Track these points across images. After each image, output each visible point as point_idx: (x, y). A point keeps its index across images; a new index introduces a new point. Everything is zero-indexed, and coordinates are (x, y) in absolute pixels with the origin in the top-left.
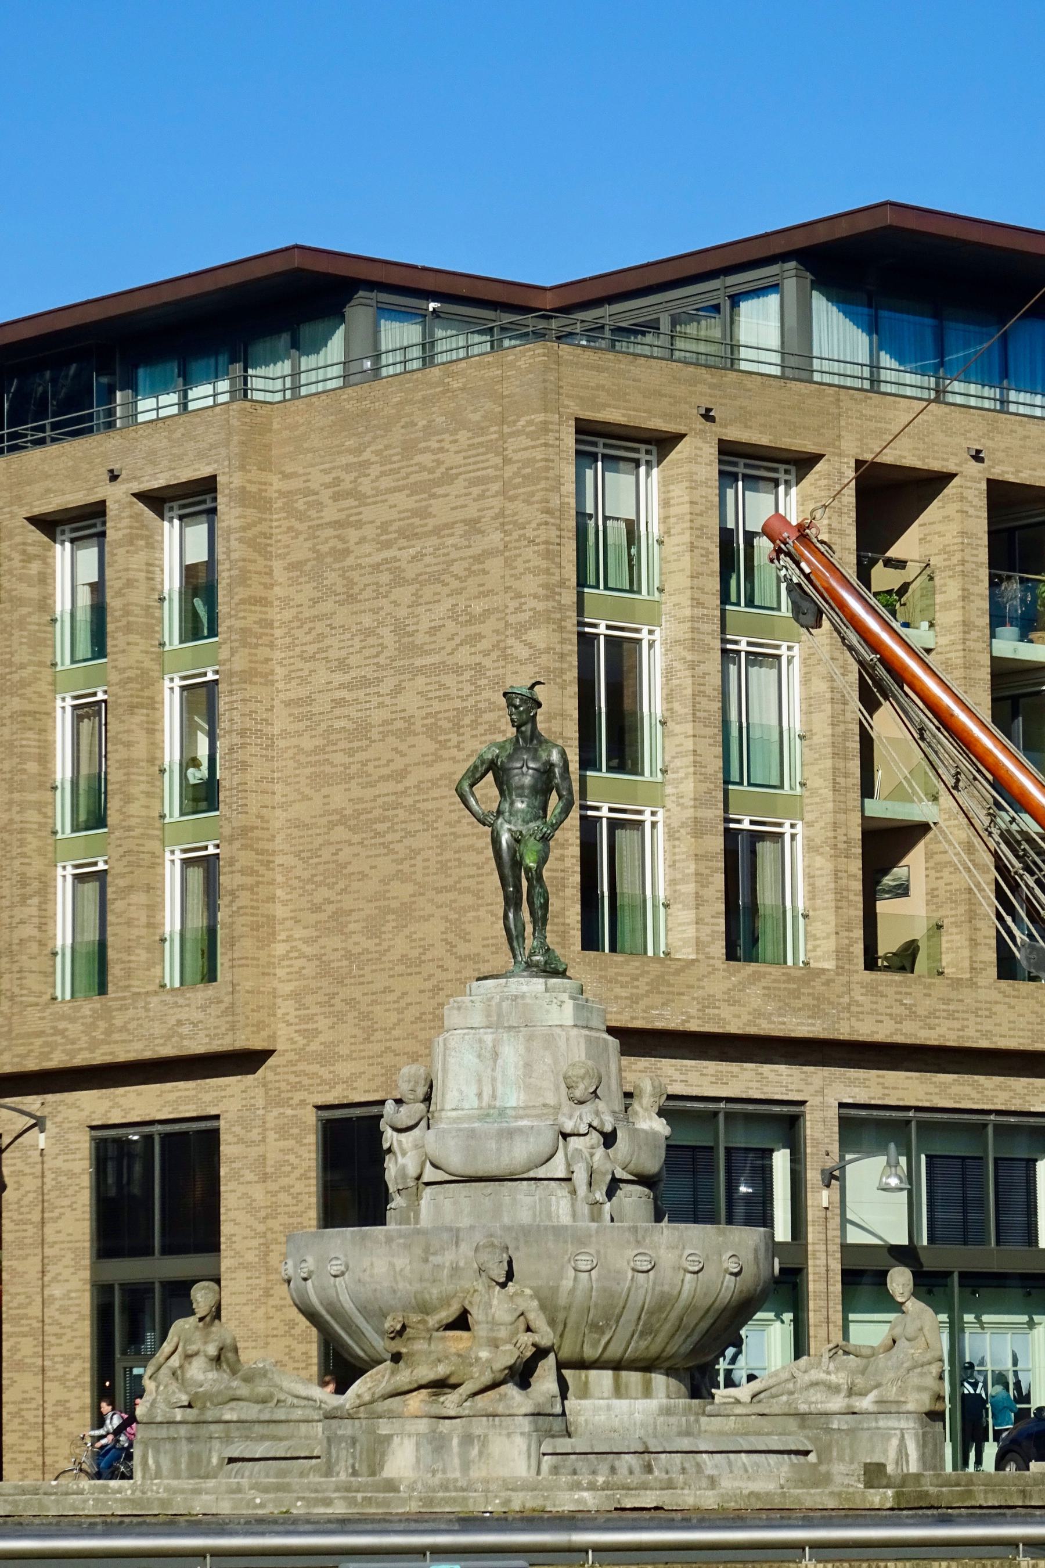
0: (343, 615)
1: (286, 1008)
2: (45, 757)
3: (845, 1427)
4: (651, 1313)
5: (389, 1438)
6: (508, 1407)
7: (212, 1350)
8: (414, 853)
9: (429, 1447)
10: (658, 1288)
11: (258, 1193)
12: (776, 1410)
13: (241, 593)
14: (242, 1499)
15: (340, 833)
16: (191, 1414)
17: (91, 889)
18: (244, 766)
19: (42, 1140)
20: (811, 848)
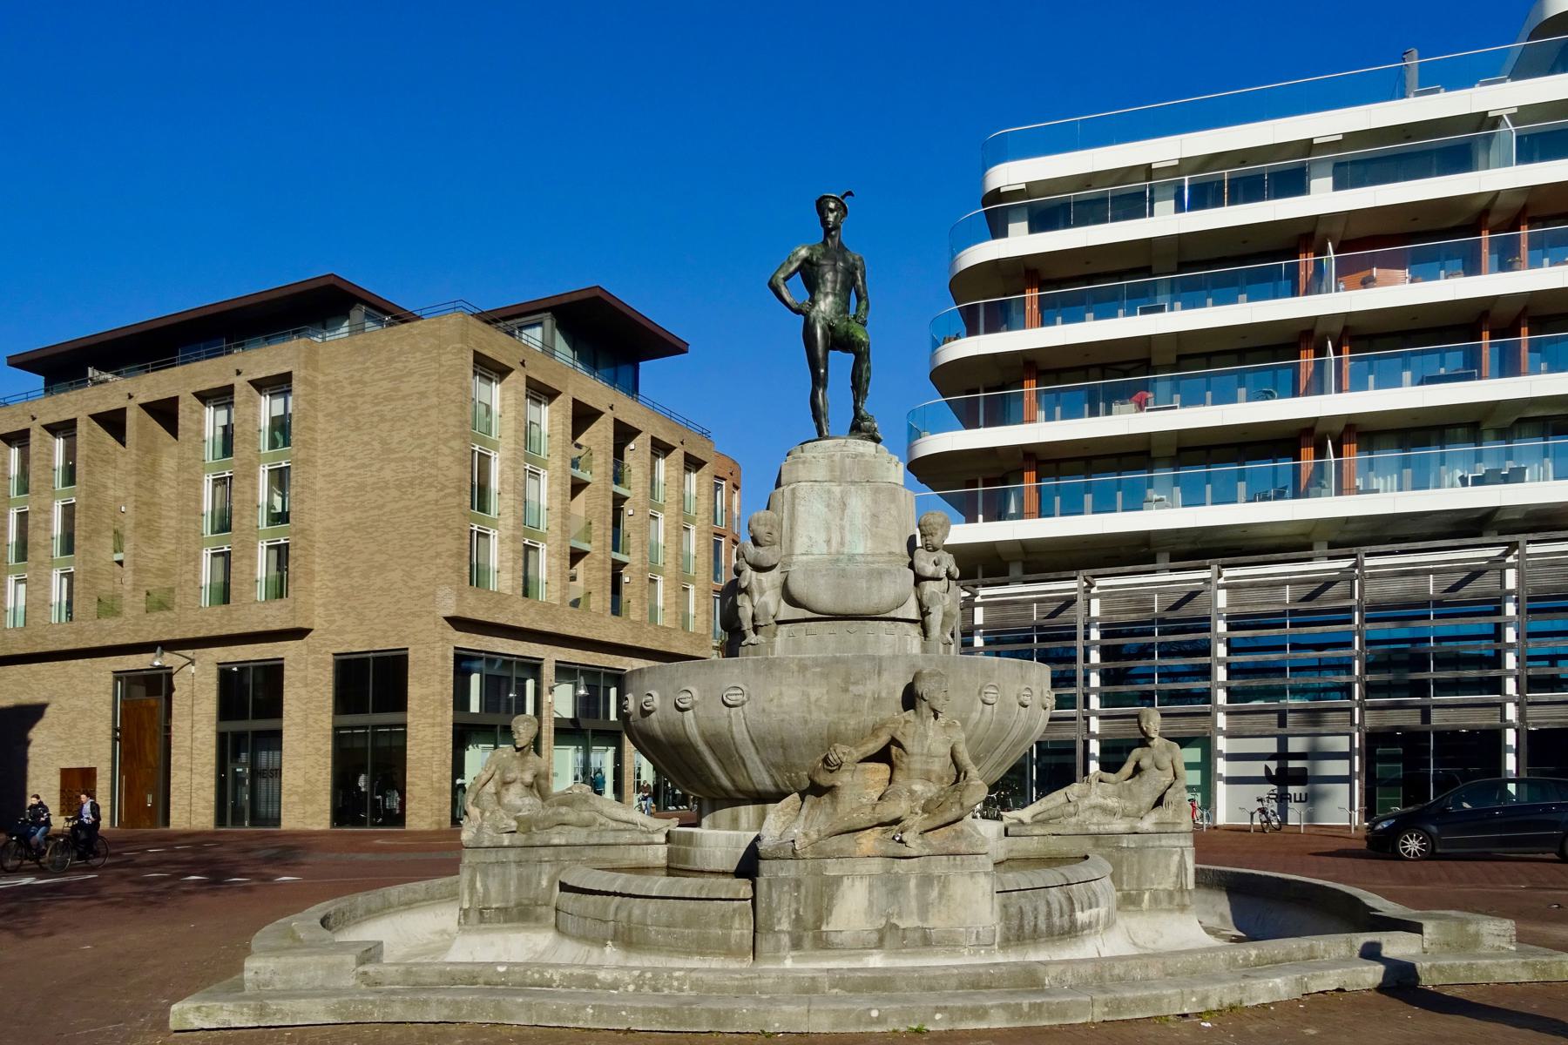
0: (353, 436)
1: (319, 610)
2: (199, 500)
5: (838, 880)
6: (970, 845)
7: (528, 778)
8: (387, 542)
9: (884, 890)
11: (303, 692)
13: (303, 424)
14: (849, 1011)
15: (350, 533)
16: (519, 839)
17: (220, 560)
18: (303, 501)
19: (193, 669)
20: (549, 554)
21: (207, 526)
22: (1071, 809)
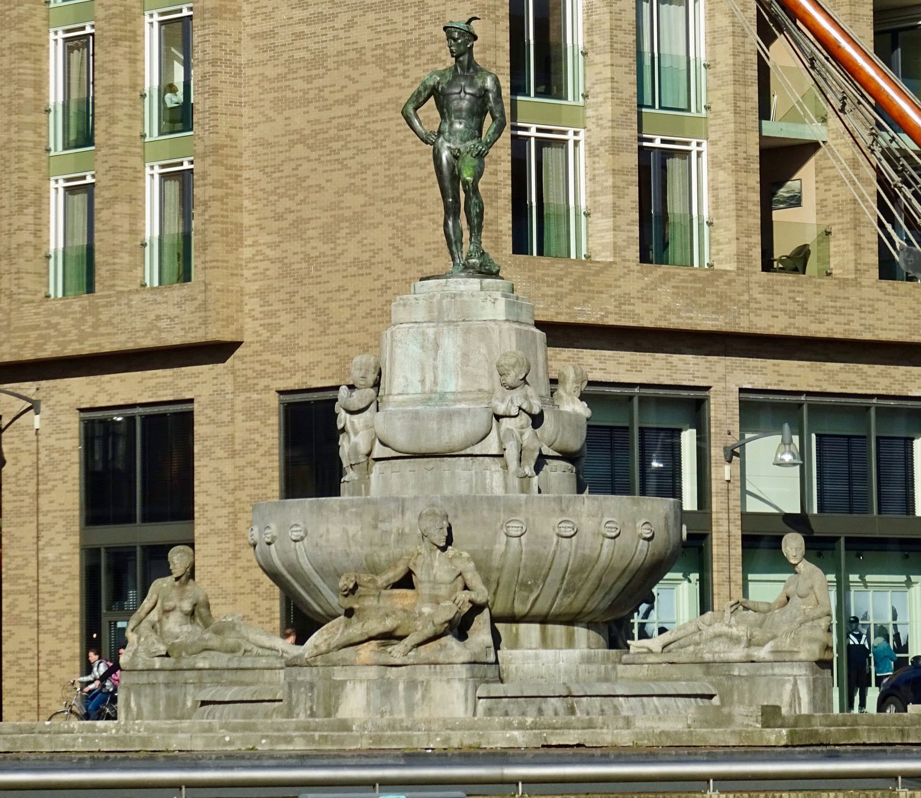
1: (252, 304)
2: (40, 84)
3: (745, 674)
4: (574, 573)
5: (343, 683)
7: (187, 606)
8: (365, 168)
10: (580, 551)
11: (227, 468)
12: (684, 659)
14: (213, 738)
15: (300, 150)
16: (169, 662)
17: (80, 200)
18: (215, 91)
19: (37, 421)
20: (715, 163)
21: (55, 132)
22: (697, 638)
